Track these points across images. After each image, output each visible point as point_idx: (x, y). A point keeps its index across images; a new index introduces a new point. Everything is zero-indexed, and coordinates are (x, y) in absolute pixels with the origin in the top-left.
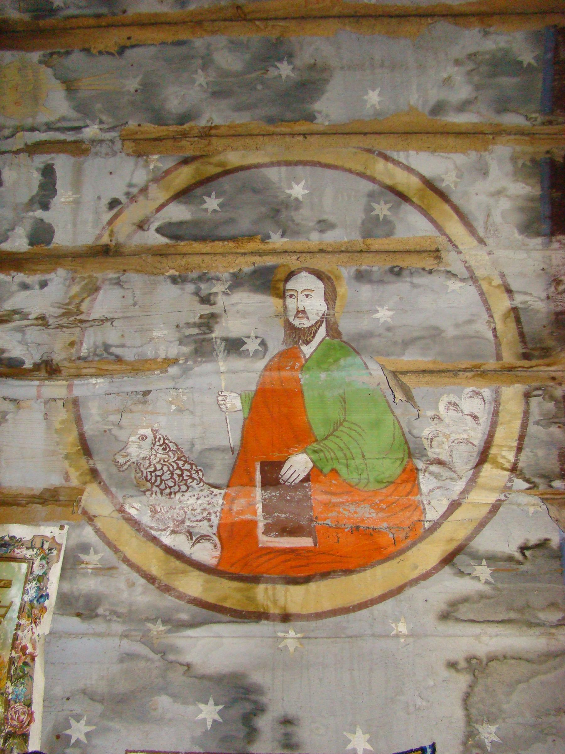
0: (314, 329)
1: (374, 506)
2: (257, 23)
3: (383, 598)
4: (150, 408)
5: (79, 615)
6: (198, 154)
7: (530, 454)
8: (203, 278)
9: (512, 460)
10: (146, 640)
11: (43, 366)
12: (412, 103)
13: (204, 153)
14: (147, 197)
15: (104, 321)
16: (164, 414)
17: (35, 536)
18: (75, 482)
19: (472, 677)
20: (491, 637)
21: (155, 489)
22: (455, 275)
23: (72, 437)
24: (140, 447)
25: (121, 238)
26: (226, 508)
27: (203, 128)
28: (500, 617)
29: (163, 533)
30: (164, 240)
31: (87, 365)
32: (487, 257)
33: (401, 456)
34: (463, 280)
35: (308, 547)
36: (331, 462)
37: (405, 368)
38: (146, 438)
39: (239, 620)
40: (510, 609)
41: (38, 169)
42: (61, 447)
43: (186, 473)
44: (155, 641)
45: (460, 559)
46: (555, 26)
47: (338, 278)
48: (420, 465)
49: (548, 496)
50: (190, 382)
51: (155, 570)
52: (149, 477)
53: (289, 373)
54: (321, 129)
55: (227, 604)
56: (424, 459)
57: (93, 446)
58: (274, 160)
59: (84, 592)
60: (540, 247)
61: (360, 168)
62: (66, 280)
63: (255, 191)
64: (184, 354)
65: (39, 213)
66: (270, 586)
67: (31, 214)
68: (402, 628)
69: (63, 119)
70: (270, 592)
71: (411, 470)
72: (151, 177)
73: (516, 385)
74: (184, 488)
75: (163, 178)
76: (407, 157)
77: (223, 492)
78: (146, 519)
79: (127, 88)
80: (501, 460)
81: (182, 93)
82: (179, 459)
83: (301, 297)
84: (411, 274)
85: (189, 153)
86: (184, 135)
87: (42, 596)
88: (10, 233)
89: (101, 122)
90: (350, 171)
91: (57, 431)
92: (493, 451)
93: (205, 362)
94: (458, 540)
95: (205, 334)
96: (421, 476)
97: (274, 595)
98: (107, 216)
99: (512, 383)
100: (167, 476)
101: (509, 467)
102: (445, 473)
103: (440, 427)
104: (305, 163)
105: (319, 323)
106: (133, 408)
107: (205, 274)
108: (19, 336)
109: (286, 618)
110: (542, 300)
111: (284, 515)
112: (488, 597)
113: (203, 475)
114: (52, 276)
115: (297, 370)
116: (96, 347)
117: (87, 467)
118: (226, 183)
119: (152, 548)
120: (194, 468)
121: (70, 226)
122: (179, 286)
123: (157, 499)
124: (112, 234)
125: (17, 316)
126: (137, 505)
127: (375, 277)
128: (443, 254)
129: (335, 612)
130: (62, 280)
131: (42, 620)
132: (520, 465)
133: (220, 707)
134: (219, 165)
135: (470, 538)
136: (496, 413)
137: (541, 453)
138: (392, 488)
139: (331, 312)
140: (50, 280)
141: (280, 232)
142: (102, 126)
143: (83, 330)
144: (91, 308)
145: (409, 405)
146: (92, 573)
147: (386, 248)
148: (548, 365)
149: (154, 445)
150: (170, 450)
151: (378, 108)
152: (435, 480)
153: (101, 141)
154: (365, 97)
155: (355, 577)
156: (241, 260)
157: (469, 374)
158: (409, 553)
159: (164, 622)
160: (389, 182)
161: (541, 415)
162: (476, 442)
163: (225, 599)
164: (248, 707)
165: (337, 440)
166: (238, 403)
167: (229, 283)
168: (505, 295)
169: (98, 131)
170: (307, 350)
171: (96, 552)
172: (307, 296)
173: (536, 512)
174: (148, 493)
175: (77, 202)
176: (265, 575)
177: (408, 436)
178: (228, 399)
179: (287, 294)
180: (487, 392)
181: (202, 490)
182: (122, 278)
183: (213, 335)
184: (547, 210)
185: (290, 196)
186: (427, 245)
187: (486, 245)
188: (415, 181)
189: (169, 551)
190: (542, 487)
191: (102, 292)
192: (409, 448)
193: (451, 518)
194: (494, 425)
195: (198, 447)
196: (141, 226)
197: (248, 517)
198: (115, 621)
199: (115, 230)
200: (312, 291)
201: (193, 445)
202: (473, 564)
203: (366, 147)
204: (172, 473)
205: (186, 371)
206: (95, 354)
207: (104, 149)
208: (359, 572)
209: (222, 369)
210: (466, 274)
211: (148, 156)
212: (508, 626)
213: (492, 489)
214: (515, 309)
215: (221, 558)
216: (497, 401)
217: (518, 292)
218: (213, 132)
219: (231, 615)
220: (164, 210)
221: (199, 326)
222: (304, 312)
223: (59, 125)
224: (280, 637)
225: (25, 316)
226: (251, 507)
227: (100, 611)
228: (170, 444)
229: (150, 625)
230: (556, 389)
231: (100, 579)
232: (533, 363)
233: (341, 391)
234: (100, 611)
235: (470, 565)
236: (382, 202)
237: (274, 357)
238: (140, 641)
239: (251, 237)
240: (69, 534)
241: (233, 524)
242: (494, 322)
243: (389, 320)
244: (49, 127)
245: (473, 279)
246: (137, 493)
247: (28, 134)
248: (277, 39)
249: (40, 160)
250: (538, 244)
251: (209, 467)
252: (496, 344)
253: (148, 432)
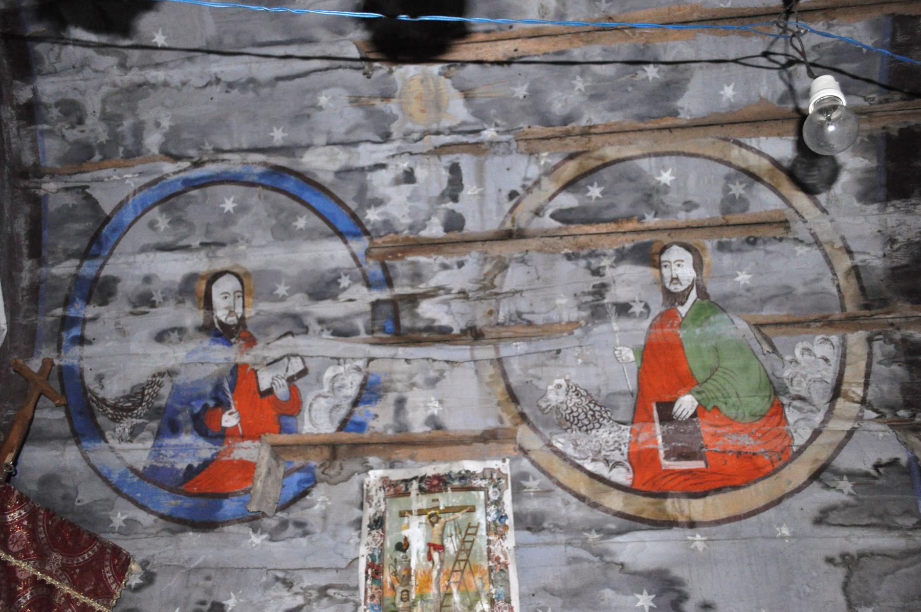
0: (687, 293)
1: (751, 435)
2: (627, 31)
3: (767, 507)
4: (561, 362)
5: (529, 529)
6: (580, 149)
7: (876, 389)
8: (593, 254)
9: (861, 394)
10: (585, 546)
11: (469, 332)
12: (762, 94)
13: (586, 149)
14: (540, 188)
15: (515, 293)
16: (573, 367)
17: (485, 469)
18: (508, 424)
19: (847, 570)
20: (859, 538)
21: (574, 427)
22: (802, 242)
23: (501, 388)
24: (557, 394)
25: (522, 224)
26: (633, 439)
27: (584, 127)
28: (865, 522)
29: (586, 461)
30: (557, 224)
31: (504, 329)
32: (829, 224)
33: (768, 394)
34: (809, 245)
35: (701, 469)
36: (711, 400)
37: (764, 321)
38: (561, 386)
39: (656, 528)
40: (872, 515)
41: (445, 168)
42: (493, 396)
43: (597, 414)
44: (593, 547)
45: (825, 475)
46: (893, 14)
47: (704, 249)
48: (785, 401)
49: (895, 423)
50: (591, 340)
51: (583, 491)
52: (568, 417)
53: (670, 330)
54: (684, 123)
55: (644, 516)
56: (788, 395)
57: (518, 394)
58: (645, 152)
59: (529, 511)
60: (877, 212)
61: (717, 155)
62: (479, 260)
63: (631, 180)
64: (583, 318)
65: (450, 205)
66: (675, 500)
67: (443, 206)
68: (785, 531)
69: (464, 123)
70: (677, 505)
71: (778, 405)
72: (542, 171)
73: (860, 332)
74: (597, 425)
75: (552, 172)
76: (759, 142)
77: (629, 427)
78: (570, 451)
79: (516, 95)
81: (564, 98)
82: (590, 402)
83: (674, 266)
84: (765, 242)
85: (573, 150)
86: (568, 134)
87: (502, 517)
88: (427, 223)
89: (497, 125)
90: (709, 158)
91: (488, 384)
92: (844, 387)
93: (601, 323)
95: (598, 300)
96: (787, 410)
97: (680, 507)
98: (508, 206)
99: (857, 330)
100: (582, 416)
101: (859, 400)
102: (807, 407)
103: (797, 369)
104: (678, 154)
105: (691, 287)
106: (547, 362)
107: (593, 251)
108: (445, 308)
109: (692, 525)
110: (879, 258)
111: (680, 445)
113: (612, 414)
114: (467, 257)
115: (676, 328)
116: (511, 315)
117: (516, 412)
118: (605, 173)
119: (578, 474)
120: (603, 409)
121: (477, 215)
122: (574, 262)
123: (576, 434)
124: (513, 221)
125: (441, 292)
126: (562, 440)
127: (734, 247)
128: (791, 224)
129: (729, 520)
130: (475, 260)
131: (507, 536)
132: (869, 398)
133: (653, 596)
134: (599, 158)
135: (832, 458)
136: (844, 355)
137: (885, 387)
138: (764, 420)
139: (700, 277)
140: (466, 261)
141: (653, 213)
142: (498, 129)
143: (498, 301)
144: (502, 282)
145: (774, 356)
146: (534, 495)
147: (741, 221)
148: (888, 313)
149: (568, 391)
150: (582, 396)
151: (732, 100)
152: (798, 413)
153: (499, 143)
154: (722, 93)
155: (742, 491)
156: (622, 238)
157: (818, 324)
158: (783, 471)
159: (598, 531)
160: (743, 165)
161: (883, 355)
162: (829, 381)
163: (642, 511)
164: (674, 596)
165: (714, 383)
166: (631, 356)
167: (614, 258)
168: (847, 256)
169: (495, 134)
170: (683, 310)
171: (534, 479)
172: (679, 265)
173: (884, 437)
174: (569, 431)
175: (482, 195)
176: (670, 492)
177: (772, 378)
178: (623, 353)
179: (663, 264)
180: (835, 339)
181: (612, 426)
182: (526, 257)
183: (606, 301)
184: (883, 180)
185: (659, 182)
186: (777, 218)
187: (828, 213)
188: (765, 163)
189: (592, 475)
190: (889, 416)
191: (510, 270)
192: (774, 387)
193: (815, 443)
194: (843, 365)
195: (604, 392)
196: (538, 213)
197: (651, 446)
198: (559, 533)
199: (516, 217)
200: (682, 261)
201: (600, 391)
203: (723, 136)
204: (586, 414)
205: (587, 331)
206: (511, 320)
207: (501, 149)
208: (744, 487)
209: (616, 328)
210: (812, 240)
211: (538, 153)
212: (871, 529)
213: (848, 419)
214: (855, 268)
215: (634, 479)
216: (844, 345)
217: (859, 253)
218: (593, 130)
219: (649, 524)
220: (557, 198)
221: (593, 294)
222: (677, 279)
223: (460, 129)
224: (688, 540)
225: (448, 291)
226: (653, 439)
227: (545, 525)
228: (582, 391)
229: (586, 534)
230: (895, 333)
231: (541, 500)
232: (873, 312)
233: (713, 343)
234: (545, 525)
235: (834, 480)
236: (737, 183)
237: (657, 317)
238: (581, 547)
239: (629, 218)
240: (510, 464)
241: (640, 452)
242: (837, 279)
243: (748, 282)
244: (452, 131)
245: (818, 243)
246: (560, 431)
247: (434, 137)
248: (644, 45)
249: (447, 160)
250: (874, 210)
251: (617, 408)
252: (840, 297)
253: (562, 381)
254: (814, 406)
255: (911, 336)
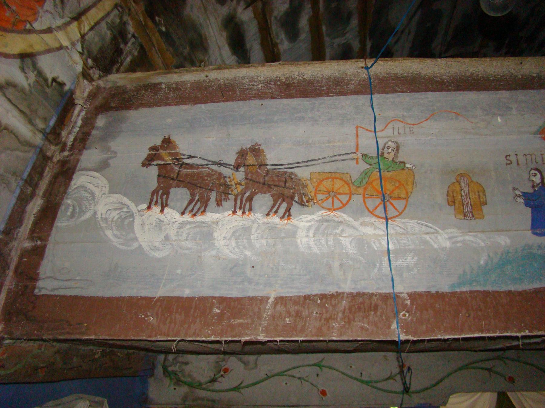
7: (93, 36)
9: (86, 31)
28: (23, 108)
30: (510, 106)
45: (28, 61)
80: (82, 27)
94: (35, 49)
102: (59, 9)
112: (24, 93)
135: (40, 53)
137: (97, 39)
152: (53, 7)
162: (82, 5)
193: (42, 35)
202: (31, 69)
254: (63, 12)
255: (129, 24)
